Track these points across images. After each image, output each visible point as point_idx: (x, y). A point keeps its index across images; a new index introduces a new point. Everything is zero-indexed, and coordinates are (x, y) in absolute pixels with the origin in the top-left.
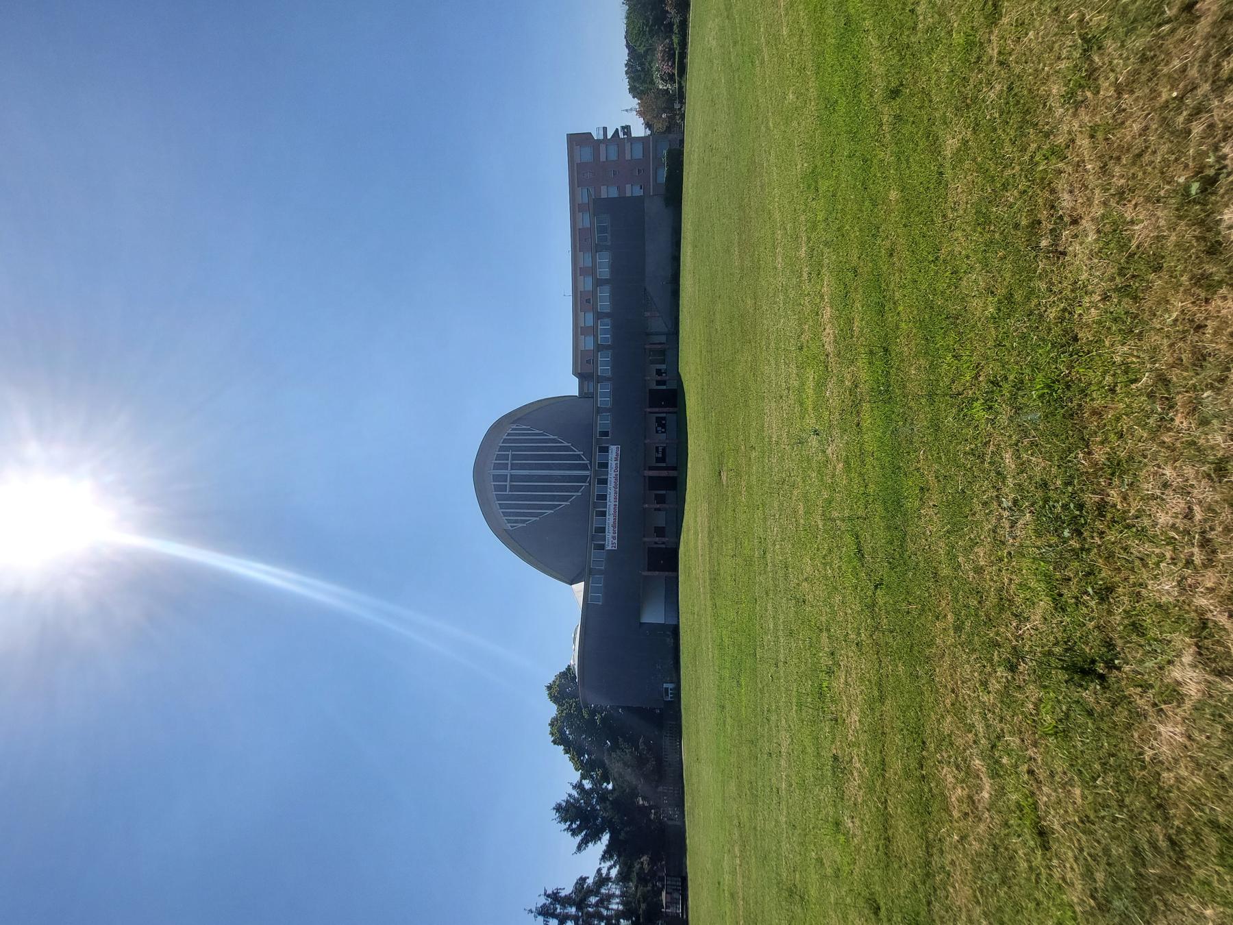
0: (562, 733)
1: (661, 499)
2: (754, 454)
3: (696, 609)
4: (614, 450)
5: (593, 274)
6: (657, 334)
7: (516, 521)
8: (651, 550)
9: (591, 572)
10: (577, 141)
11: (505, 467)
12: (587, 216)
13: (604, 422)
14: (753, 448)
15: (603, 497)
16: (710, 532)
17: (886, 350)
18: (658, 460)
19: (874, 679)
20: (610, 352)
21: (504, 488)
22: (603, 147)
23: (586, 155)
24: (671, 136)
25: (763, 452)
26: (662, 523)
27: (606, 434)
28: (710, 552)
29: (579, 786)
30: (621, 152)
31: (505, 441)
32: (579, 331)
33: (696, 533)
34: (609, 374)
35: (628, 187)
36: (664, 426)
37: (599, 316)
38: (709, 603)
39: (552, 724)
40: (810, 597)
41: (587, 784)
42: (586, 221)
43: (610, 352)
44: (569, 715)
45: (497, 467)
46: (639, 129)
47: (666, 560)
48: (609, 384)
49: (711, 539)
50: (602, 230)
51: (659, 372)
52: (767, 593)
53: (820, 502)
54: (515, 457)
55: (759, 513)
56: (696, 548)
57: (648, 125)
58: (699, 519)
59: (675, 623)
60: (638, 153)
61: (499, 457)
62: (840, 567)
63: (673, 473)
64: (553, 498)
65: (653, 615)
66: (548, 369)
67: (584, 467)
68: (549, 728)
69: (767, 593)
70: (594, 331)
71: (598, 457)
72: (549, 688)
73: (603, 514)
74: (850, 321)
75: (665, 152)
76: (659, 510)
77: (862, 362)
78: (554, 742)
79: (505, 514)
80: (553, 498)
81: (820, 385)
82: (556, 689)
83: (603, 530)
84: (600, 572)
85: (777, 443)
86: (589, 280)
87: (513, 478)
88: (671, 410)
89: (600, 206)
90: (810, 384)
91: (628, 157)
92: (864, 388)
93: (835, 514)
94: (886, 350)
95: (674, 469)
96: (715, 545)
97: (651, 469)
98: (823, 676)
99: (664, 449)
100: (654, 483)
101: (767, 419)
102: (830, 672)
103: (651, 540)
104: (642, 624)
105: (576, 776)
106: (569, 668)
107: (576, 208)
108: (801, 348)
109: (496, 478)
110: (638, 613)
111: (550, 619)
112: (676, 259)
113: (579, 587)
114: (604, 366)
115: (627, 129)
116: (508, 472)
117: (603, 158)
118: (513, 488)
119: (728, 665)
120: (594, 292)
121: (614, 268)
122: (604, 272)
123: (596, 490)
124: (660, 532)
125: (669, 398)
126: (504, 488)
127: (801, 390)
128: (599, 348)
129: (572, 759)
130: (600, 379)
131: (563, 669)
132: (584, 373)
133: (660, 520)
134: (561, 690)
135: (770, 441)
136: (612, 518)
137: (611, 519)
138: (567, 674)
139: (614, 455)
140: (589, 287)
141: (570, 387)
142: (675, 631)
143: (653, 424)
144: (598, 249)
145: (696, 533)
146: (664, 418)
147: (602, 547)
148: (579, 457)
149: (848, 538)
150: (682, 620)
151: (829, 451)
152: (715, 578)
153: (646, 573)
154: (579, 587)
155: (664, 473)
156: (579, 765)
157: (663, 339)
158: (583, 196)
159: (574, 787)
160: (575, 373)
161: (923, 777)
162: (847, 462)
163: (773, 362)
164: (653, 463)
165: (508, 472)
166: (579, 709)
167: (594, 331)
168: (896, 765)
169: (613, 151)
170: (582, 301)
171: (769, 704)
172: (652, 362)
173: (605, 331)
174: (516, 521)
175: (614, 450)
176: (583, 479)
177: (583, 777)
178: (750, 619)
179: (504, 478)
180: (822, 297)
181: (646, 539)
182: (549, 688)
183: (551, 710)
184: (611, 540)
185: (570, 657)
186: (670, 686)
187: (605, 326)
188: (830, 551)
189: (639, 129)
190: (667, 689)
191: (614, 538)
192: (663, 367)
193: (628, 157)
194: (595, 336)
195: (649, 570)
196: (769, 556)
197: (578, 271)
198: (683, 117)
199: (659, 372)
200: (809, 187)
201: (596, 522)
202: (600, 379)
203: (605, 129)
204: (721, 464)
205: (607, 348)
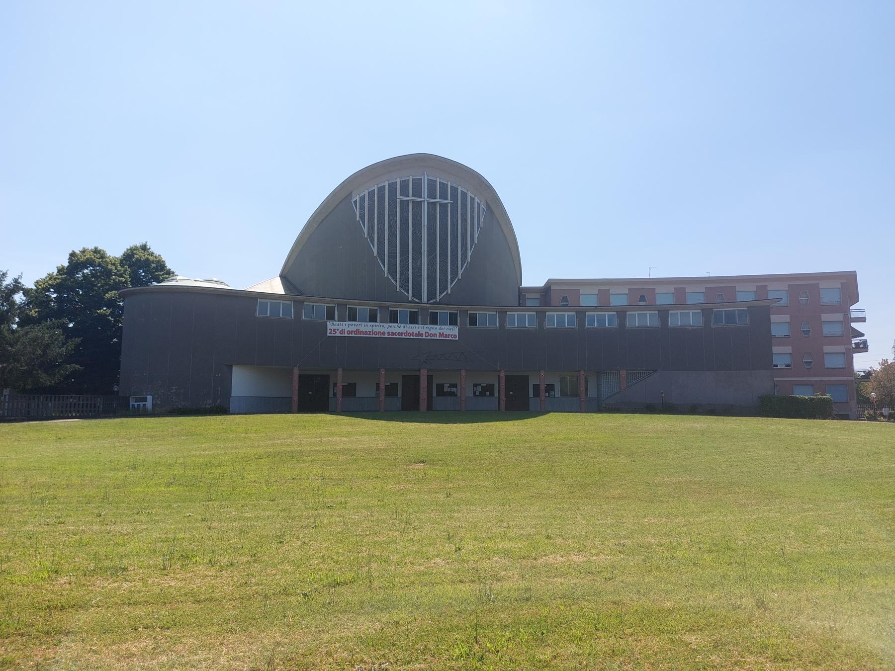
0: (88, 263)
1: (391, 390)
2: (441, 496)
3: (252, 435)
4: (452, 332)
5: (675, 306)
6: (598, 385)
7: (362, 208)
8: (325, 379)
9: (298, 303)
10: (847, 286)
11: (432, 194)
12: (751, 297)
13: (487, 318)
14: (449, 495)
15: (394, 318)
16: (350, 450)
17: (527, 600)
18: (440, 387)
19: (217, 595)
20: (575, 326)
21: (404, 193)
22: (839, 317)
23: (829, 296)
24: (853, 404)
25: (442, 506)
26: (360, 393)
27: (473, 321)
28: (325, 452)
29: (17, 287)
30: (833, 340)
31: (464, 195)
32: (604, 287)
33: (348, 434)
34: (547, 326)
35: (789, 349)
36: (482, 394)
37: (621, 313)
38: (261, 451)
39: (96, 251)
40: (286, 547)
41: (19, 298)
42: (746, 296)
43: (575, 326)
44: (108, 273)
45: (432, 184)
46: (862, 363)
47: (314, 396)
48: (535, 325)
49: (343, 452)
50: (730, 316)
51: (550, 388)
52: (284, 510)
53: (385, 553)
54: (444, 206)
55: (376, 502)
56: (331, 434)
57: (868, 374)
58: (366, 438)
59: (233, 406)
60: (831, 362)
61: (443, 186)
62: (320, 570)
63: (423, 405)
64: (392, 256)
65: (242, 382)
66: (553, 250)
67: (432, 294)
68: (91, 247)
69: (284, 510)
70: (604, 305)
71: (444, 312)
72: (144, 248)
73: (373, 319)
74: (564, 575)
75: (827, 396)
76: (378, 385)
77: (523, 584)
78: (73, 255)
79: (371, 194)
80: (392, 256)
81: (506, 553)
82: (140, 255)
83: (352, 317)
84: (298, 314)
85: (451, 518)
86: (668, 300)
87: (418, 205)
88: (503, 403)
89: (760, 315)
90: (508, 545)
91: (827, 349)
92: (496, 586)
93: (374, 566)
94: (527, 600)
95: (430, 407)
96: (335, 458)
97: (430, 378)
98: (208, 557)
99: (452, 394)
100: (411, 382)
101: (479, 508)
102: (212, 563)
103: (340, 379)
104: (230, 367)
105: (29, 283)
106: (169, 273)
107: (761, 283)
108: (548, 537)
109: (417, 184)
110: (240, 363)
111: (234, 249)
112: (694, 409)
113: (278, 288)
114: (556, 319)
115: (863, 347)
116: (425, 198)
117: (825, 317)
118: (404, 204)
119: (190, 473)
120: (652, 306)
121: (682, 332)
122: (676, 320)
123: (403, 309)
124: (350, 390)
125: (517, 398)
126: (404, 193)
127: (504, 537)
128: (581, 313)
129: (50, 277)
130: (541, 315)
131: (169, 265)
132: (546, 293)
133: (365, 391)
134: (143, 266)
135: (454, 511)
136: (369, 329)
137: (365, 328)
138: (159, 269)
139: (446, 332)
140: (661, 300)
141: (533, 277)
142: (222, 410)
143: (484, 381)
144: (706, 312)
145: (348, 434)
146: (492, 394)
147: (331, 317)
148: (444, 288)
149: (350, 575)
150: (237, 418)
151: (438, 560)
152: (296, 456)
153: (296, 372)
154: (278, 288)
155: (423, 394)
156: (42, 288)
157: (592, 393)
158: (775, 292)
159: (16, 281)
160: (550, 283)
161: (136, 629)
162: (425, 574)
163: (541, 513)
164: (436, 381)
165: (425, 198)
166: (116, 286)
167: (604, 305)
168: (139, 611)
169: (837, 330)
170: (642, 291)
171: (156, 514)
172: (562, 380)
173: (601, 320)
174: (362, 208)
175: (452, 332)
176: (417, 294)
177: (26, 292)
178: (250, 495)
179: (418, 192)
180: (596, 555)
181: (340, 372)
182: (144, 248)
183: (115, 251)
184: (338, 328)
185: (188, 273)
186: (149, 404)
187: (608, 319)
188: (336, 562)
189: (862, 363)
190: (145, 400)
191: (343, 331)
192: (557, 393)
193: (827, 349)
194: (595, 309)
195: (300, 376)
196: (327, 511)
197: (680, 285)
198: (872, 418)
199: (550, 388)
200: (716, 545)
201: (363, 308)
202: (541, 315)
203: (863, 320)
204: (433, 463)
205: (581, 323)
